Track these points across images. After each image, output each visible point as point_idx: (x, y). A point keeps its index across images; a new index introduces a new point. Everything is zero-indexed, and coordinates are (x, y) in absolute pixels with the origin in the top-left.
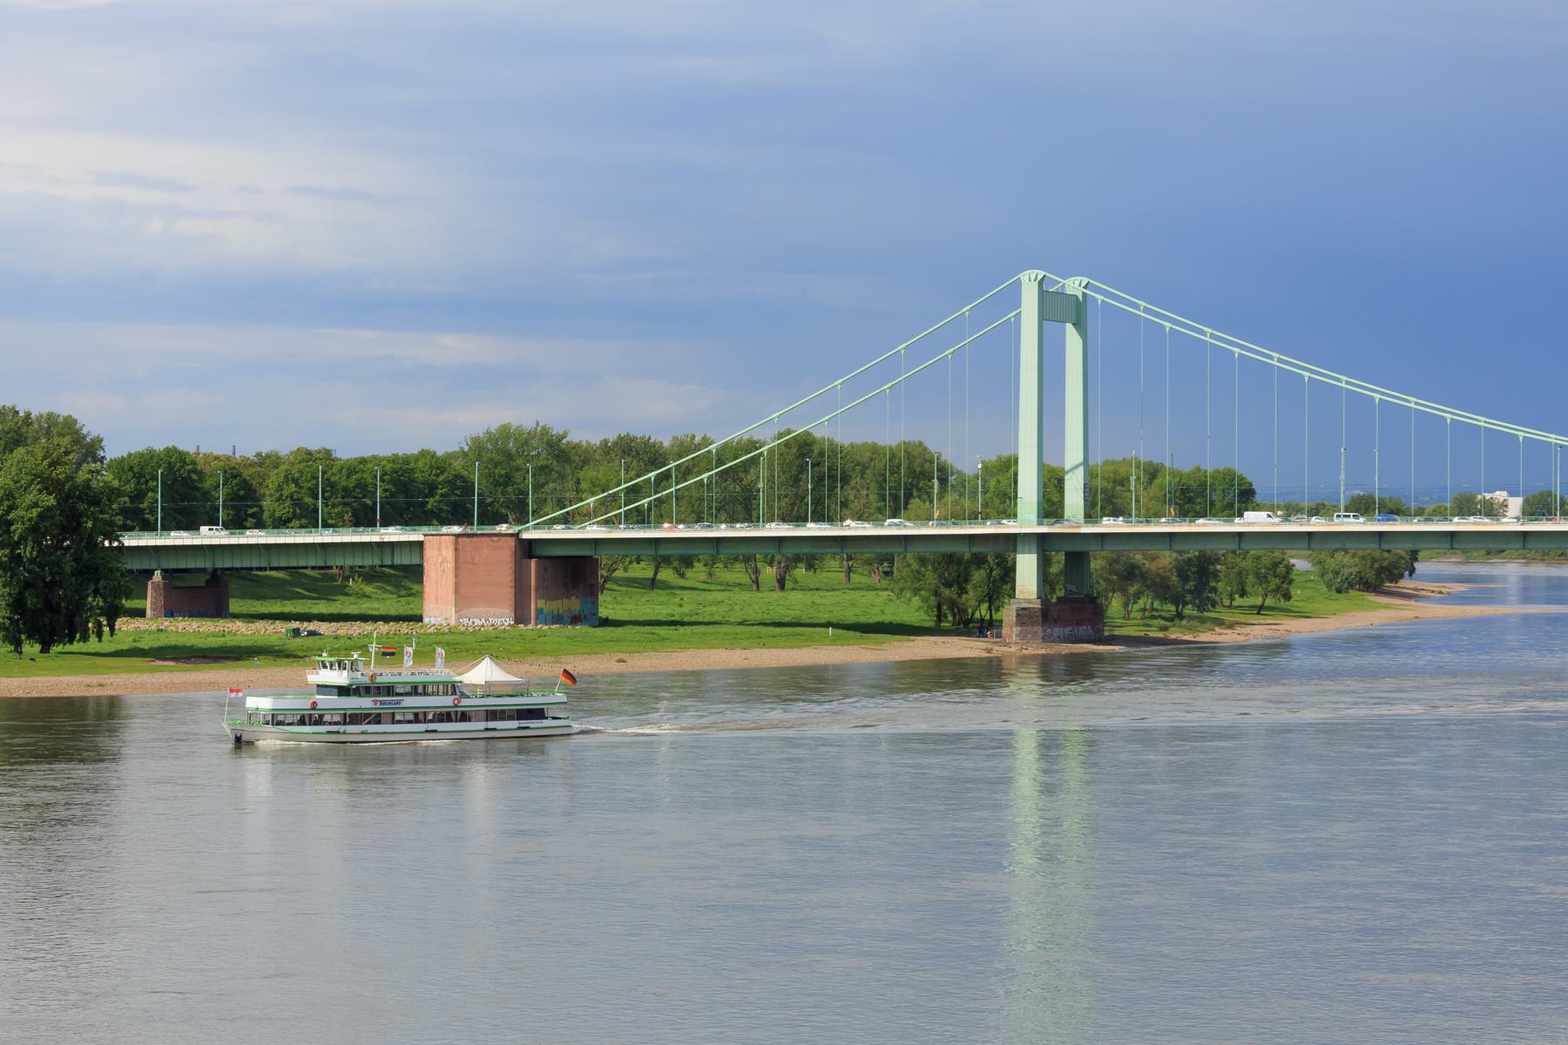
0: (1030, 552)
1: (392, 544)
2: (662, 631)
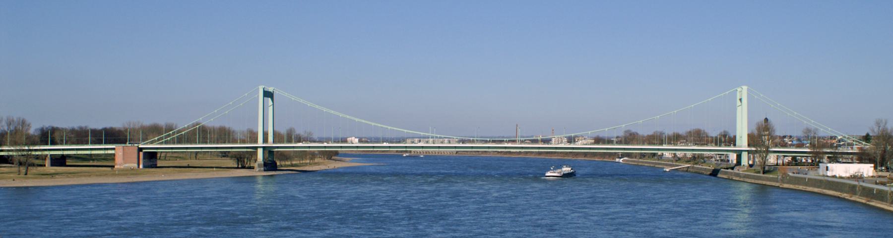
2: (43, 176)
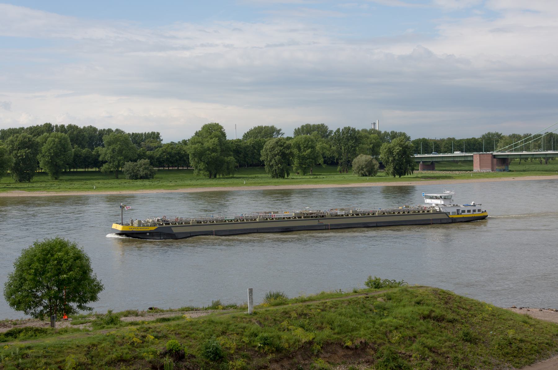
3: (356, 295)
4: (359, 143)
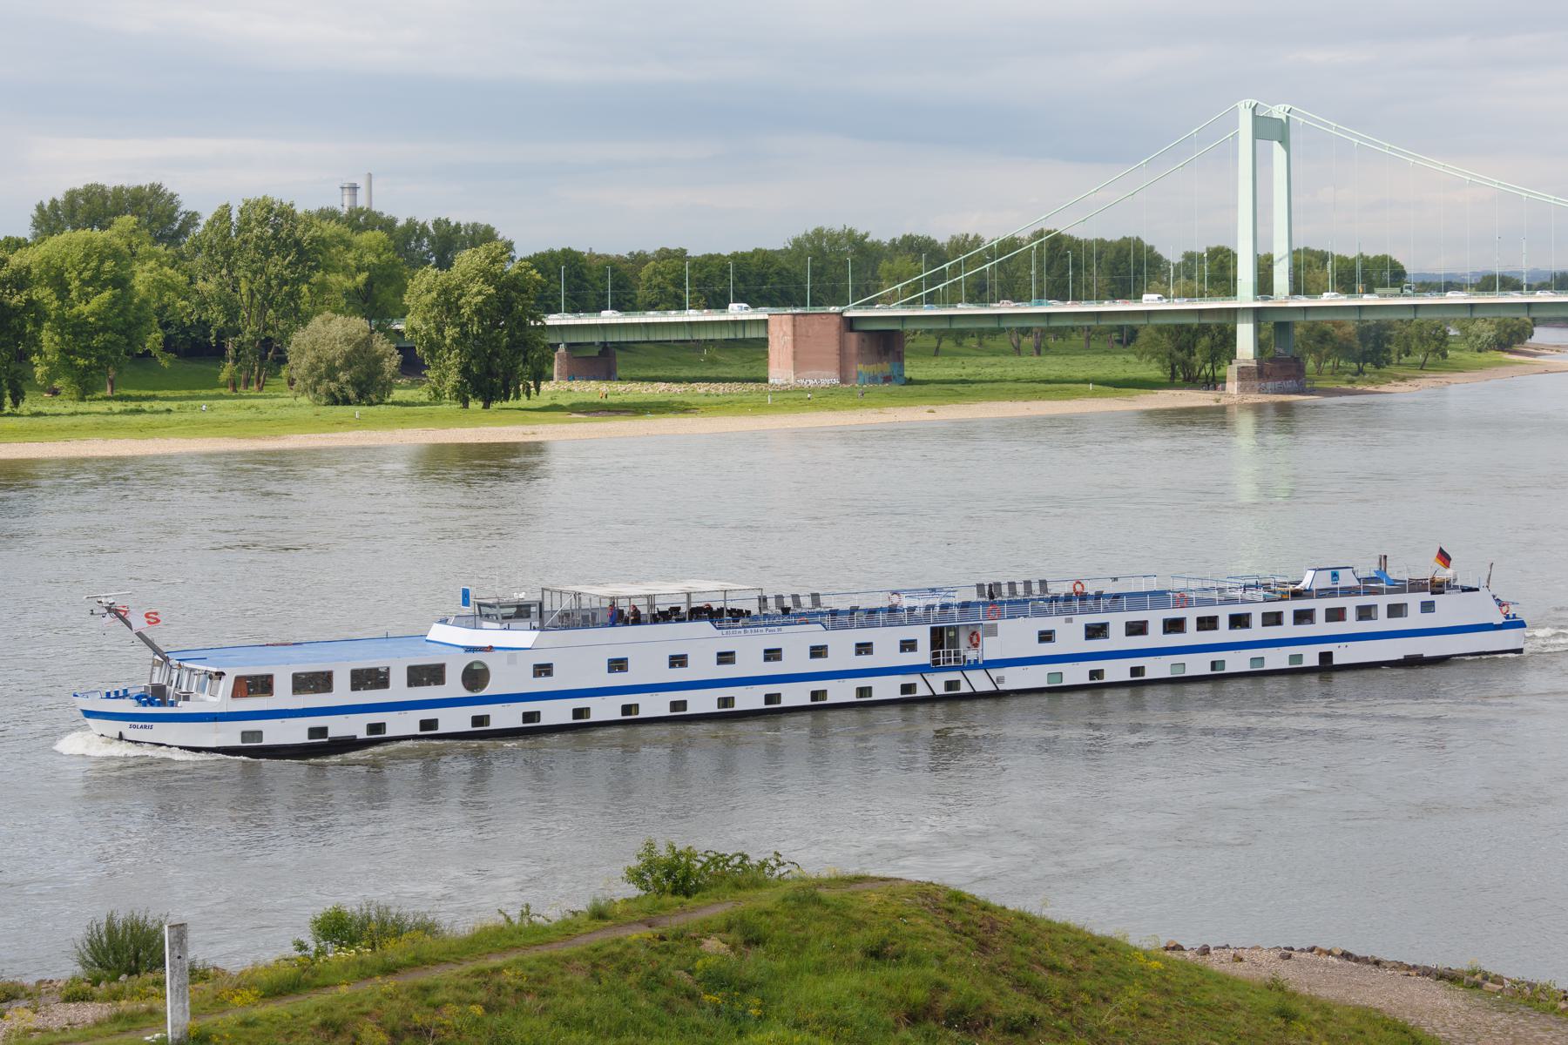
0: (1248, 322)
1: (744, 322)
2: (958, 387)
3: (605, 928)
4: (311, 268)
